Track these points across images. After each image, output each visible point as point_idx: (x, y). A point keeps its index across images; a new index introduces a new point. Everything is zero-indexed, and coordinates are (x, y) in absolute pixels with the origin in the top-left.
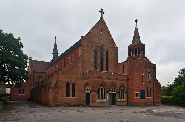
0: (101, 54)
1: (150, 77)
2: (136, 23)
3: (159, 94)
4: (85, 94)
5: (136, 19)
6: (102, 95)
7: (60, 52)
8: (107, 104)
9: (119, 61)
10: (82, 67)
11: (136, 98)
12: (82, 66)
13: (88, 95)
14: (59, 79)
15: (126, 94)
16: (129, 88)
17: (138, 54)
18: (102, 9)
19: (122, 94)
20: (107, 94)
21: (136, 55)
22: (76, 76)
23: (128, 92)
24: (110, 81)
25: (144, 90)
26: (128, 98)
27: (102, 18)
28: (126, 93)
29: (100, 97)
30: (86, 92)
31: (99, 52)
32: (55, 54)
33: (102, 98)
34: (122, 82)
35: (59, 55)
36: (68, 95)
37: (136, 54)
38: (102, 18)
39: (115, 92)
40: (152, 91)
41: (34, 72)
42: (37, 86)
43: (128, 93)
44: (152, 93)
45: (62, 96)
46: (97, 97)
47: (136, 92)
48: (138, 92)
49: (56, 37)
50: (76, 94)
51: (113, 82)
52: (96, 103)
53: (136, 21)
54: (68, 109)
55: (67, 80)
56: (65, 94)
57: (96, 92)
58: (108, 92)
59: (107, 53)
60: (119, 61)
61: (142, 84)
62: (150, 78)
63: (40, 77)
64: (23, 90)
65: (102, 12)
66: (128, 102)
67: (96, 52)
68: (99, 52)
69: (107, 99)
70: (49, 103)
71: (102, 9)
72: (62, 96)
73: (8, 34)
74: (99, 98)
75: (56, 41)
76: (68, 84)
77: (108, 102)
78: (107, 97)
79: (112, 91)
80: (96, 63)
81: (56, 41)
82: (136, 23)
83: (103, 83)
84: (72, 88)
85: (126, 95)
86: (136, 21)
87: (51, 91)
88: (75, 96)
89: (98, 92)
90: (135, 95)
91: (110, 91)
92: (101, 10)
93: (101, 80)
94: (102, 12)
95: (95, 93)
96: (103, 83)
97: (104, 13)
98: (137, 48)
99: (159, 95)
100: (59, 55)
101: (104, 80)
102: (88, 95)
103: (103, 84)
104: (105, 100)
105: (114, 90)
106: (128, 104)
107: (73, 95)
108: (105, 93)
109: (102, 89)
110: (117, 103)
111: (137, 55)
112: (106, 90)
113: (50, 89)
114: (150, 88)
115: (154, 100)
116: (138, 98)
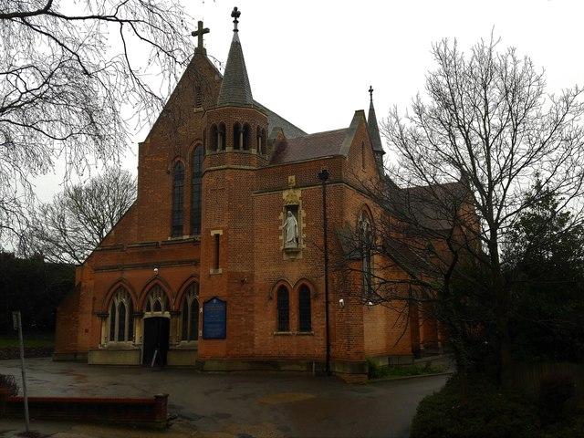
2: (236, 22)
5: (236, 9)
8: (132, 359)
17: (245, 148)
19: (122, 317)
21: (237, 151)
27: (200, 51)
30: (148, 315)
36: (283, 323)
39: (167, 314)
40: (316, 296)
44: (317, 305)
46: (105, 331)
51: (156, 277)
52: (97, 354)
53: (236, 14)
54: (386, 381)
61: (211, 271)
69: (137, 341)
74: (184, 338)
75: (371, 103)
78: (139, 332)
79: (158, 308)
80: (177, 212)
81: (371, 103)
82: (236, 22)
101: (127, 275)
103: (119, 288)
104: (127, 343)
109: (122, 304)
110: (173, 359)
111: (242, 149)
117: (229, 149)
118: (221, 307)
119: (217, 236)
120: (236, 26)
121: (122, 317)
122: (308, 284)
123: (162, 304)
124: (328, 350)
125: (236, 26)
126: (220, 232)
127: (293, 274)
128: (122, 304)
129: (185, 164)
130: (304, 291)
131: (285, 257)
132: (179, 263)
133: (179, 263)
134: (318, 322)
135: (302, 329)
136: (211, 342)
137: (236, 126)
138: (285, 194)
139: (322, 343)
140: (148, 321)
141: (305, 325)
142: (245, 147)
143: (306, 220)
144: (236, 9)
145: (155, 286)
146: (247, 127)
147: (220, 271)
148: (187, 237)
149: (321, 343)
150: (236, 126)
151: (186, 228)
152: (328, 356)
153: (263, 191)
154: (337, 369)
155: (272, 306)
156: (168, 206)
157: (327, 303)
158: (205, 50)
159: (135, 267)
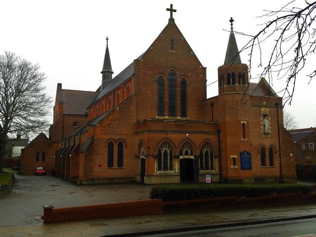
0: (171, 86)
1: (266, 125)
2: (232, 24)
3: (290, 158)
4: (140, 161)
5: (231, 18)
6: (166, 163)
7: (117, 69)
9: (209, 96)
10: (135, 113)
11: (232, 167)
12: (135, 111)
13: (143, 161)
14: (96, 137)
15: (217, 160)
16: (221, 148)
18: (171, 6)
20: (177, 160)
22: (124, 129)
23: (220, 155)
24: (181, 136)
25: (247, 152)
26: (220, 167)
27: (172, 20)
28: (216, 157)
29: (163, 166)
30: (181, 157)
31: (166, 86)
32: (107, 74)
33: (166, 169)
34: (207, 137)
35: (114, 76)
37: (229, 84)
38: (172, 20)
39: (192, 157)
41: (64, 115)
42: (77, 143)
43: (219, 157)
44: (276, 156)
45: (100, 166)
46: (156, 166)
47: (232, 157)
48: (236, 157)
49: (107, 39)
50: (125, 161)
51: (188, 138)
53: (232, 21)
55: (108, 137)
56: (105, 163)
57: (153, 156)
58: (177, 157)
59: (184, 83)
60: (209, 96)
61: (243, 140)
62: (267, 128)
63: (75, 124)
64: (44, 154)
65: (171, 10)
66: (221, 177)
67: (161, 83)
68: (166, 86)
70: (78, 177)
71: (171, 6)
72: (100, 166)
73: (22, 59)
74: (160, 169)
75: (107, 46)
76: (111, 145)
77: (177, 175)
78: (177, 166)
79: (187, 154)
81: (107, 46)
82: (232, 24)
83: (167, 140)
84: (114, 153)
85: (216, 162)
86: (232, 21)
87: (82, 157)
88: (124, 165)
89: (158, 157)
90: (230, 162)
91: (181, 154)
92: (169, 8)
93: (164, 135)
94: (171, 10)
95: (152, 159)
96: (167, 140)
97: (175, 11)
98: (233, 72)
99: (292, 160)
100: (114, 76)
101: (169, 136)
102: (143, 161)
103: (167, 142)
105: (190, 152)
106: (220, 180)
107: (120, 164)
108: (171, 160)
109: (166, 151)
112: (214, 154)
113: (81, 155)
114: (267, 145)
115: (281, 171)
116: (237, 167)
117: (237, 85)
118: (248, 156)
119: (244, 124)
120: (232, 26)
121: (166, 158)
122: (272, 147)
123: (190, 152)
124: (281, 173)
125: (232, 26)
126: (246, 122)
127: (267, 143)
128: (166, 151)
129: (166, 79)
130: (271, 149)
131: (263, 136)
132: (200, 132)
133: (200, 132)
134: (276, 162)
135: (270, 165)
136: (246, 171)
137: (229, 74)
138: (263, 109)
139: (279, 170)
140: (181, 160)
141: (272, 164)
142: (234, 83)
143: (271, 121)
144: (231, 18)
145: (188, 143)
146: (233, 74)
147: (247, 140)
148: (167, 117)
149: (278, 170)
150: (229, 74)
151: (166, 112)
152: (281, 175)
153: (254, 106)
154: (285, 180)
155: (259, 156)
156: (156, 98)
157: (280, 155)
158: (174, 19)
159: (174, 132)
